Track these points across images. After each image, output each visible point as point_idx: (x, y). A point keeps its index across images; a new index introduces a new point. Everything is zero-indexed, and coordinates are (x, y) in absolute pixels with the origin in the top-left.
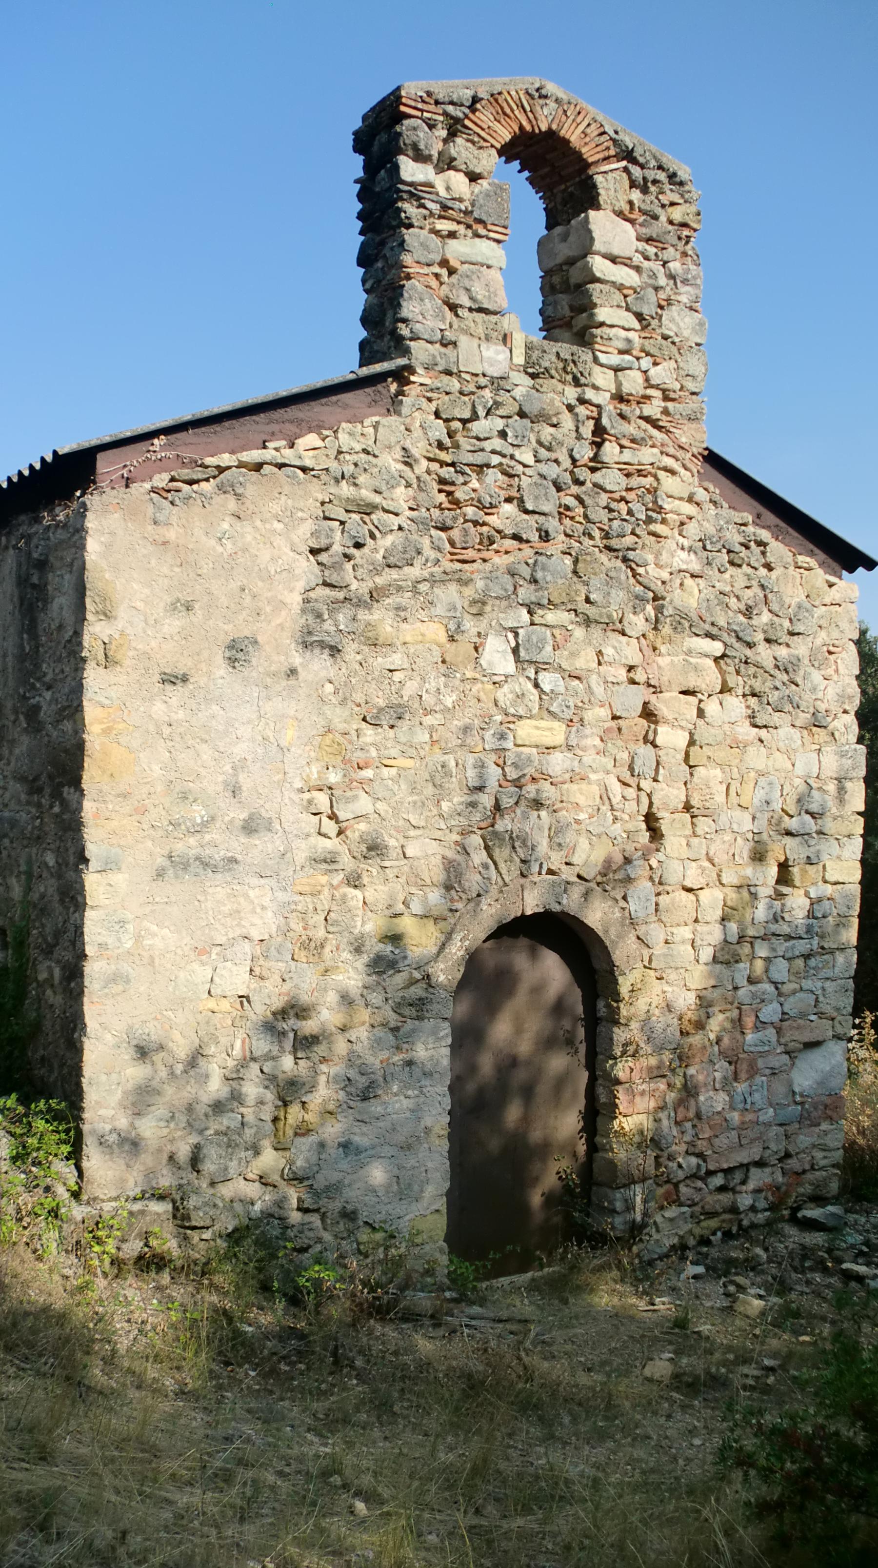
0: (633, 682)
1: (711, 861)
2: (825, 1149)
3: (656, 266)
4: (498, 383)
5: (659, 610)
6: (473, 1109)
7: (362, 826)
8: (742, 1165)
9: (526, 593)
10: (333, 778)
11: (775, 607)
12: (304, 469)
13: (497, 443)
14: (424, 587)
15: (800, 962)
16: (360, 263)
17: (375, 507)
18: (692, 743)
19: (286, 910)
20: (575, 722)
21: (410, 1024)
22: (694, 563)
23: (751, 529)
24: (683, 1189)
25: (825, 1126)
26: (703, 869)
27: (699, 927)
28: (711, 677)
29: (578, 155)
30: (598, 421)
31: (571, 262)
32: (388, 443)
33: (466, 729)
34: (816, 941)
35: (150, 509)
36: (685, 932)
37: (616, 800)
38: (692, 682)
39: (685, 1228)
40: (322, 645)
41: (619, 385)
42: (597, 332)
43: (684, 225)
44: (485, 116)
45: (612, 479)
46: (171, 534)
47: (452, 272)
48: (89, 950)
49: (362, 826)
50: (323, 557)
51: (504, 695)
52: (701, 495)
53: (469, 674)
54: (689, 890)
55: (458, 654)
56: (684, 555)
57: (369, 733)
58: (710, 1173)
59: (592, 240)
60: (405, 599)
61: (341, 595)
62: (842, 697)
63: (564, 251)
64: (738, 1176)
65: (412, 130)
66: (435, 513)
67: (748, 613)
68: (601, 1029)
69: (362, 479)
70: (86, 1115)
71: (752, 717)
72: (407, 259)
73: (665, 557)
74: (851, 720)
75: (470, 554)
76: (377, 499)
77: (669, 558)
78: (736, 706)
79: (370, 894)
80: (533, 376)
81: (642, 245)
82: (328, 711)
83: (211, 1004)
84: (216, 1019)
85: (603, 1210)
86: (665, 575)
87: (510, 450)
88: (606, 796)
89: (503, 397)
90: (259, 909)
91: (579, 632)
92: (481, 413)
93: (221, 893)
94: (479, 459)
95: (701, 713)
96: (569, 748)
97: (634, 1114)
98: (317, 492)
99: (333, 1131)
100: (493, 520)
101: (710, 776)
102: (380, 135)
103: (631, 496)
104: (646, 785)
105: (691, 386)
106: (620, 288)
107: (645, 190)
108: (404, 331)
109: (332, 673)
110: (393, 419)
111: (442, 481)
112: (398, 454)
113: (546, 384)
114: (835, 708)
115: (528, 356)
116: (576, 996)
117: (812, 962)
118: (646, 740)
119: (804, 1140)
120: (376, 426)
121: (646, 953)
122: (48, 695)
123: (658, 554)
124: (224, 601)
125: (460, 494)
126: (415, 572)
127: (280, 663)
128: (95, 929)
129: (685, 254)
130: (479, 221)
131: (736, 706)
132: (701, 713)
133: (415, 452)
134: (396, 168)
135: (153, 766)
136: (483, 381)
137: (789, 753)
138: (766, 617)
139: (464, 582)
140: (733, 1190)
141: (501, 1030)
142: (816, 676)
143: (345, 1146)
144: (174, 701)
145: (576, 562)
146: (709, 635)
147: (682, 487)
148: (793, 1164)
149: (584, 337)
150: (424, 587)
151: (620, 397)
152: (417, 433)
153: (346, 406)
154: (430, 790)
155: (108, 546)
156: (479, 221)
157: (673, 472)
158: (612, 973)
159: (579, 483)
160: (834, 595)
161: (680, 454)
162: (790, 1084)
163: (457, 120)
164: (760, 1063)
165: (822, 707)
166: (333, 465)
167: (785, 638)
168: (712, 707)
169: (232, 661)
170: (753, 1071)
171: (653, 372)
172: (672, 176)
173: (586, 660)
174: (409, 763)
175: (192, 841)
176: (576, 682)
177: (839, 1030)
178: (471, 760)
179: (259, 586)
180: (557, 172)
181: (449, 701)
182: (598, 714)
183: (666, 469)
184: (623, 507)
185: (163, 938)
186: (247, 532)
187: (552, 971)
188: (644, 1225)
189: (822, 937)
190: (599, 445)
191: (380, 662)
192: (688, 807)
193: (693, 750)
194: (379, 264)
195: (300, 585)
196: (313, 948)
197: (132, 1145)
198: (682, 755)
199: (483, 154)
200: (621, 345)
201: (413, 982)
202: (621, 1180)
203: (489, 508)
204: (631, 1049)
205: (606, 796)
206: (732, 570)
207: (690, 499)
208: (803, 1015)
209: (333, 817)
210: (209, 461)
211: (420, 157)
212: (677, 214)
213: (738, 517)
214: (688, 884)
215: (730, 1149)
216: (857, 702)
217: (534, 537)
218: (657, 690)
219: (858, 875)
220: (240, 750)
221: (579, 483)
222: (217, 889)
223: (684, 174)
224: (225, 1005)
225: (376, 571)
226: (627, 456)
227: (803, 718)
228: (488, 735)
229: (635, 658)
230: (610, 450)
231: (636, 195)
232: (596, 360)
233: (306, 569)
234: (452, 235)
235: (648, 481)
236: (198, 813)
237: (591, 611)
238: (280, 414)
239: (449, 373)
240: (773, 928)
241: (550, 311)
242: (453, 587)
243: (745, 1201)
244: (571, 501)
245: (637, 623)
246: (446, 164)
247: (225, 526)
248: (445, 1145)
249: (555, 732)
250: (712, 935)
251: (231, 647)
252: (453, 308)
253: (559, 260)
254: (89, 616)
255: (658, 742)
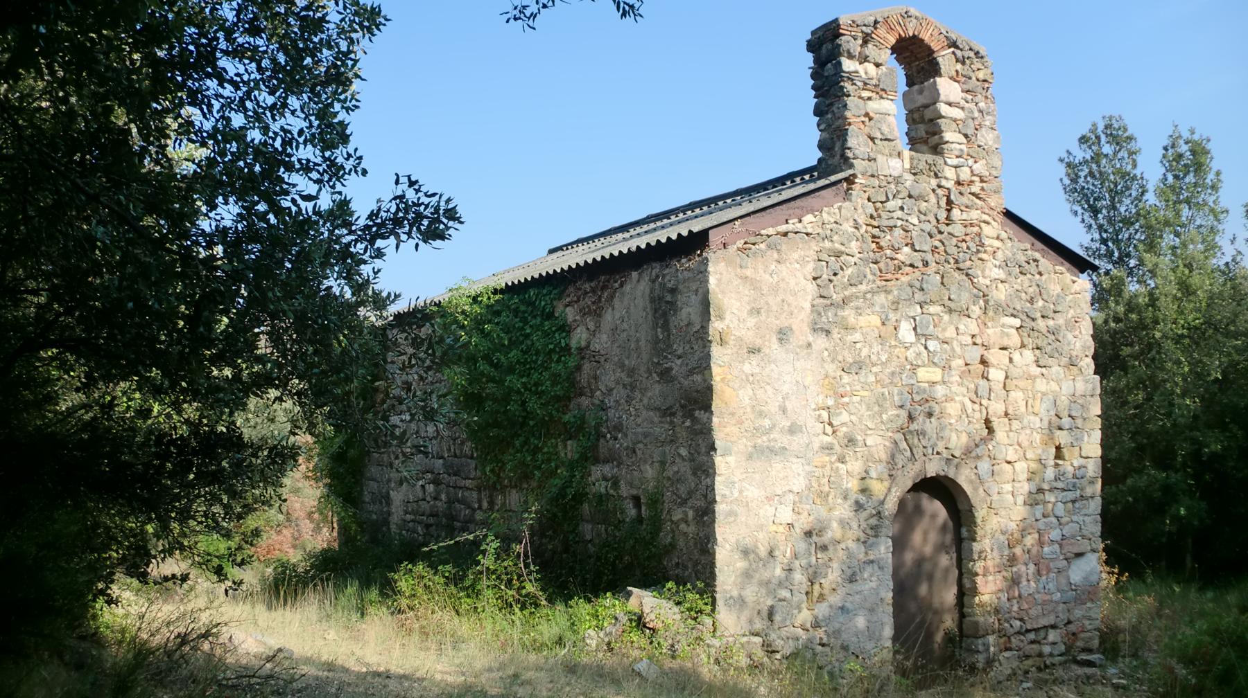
0: (975, 344)
1: (1019, 445)
2: (1090, 618)
3: (972, 106)
4: (898, 180)
5: (986, 302)
6: (904, 588)
7: (844, 429)
8: (1045, 627)
9: (919, 296)
10: (830, 402)
11: (1045, 297)
12: (807, 234)
13: (899, 214)
14: (869, 296)
15: (1070, 505)
16: (816, 114)
17: (842, 253)
18: (1007, 377)
19: (810, 474)
20: (946, 368)
21: (872, 540)
22: (1001, 274)
23: (1029, 252)
24: (1013, 639)
25: (1089, 605)
26: (1016, 451)
27: (1017, 485)
28: (1015, 340)
29: (929, 48)
30: (948, 197)
31: (926, 106)
32: (839, 217)
33: (893, 373)
34: (1078, 492)
35: (738, 260)
36: (1008, 487)
37: (969, 411)
38: (1006, 343)
39: (1015, 664)
40: (822, 329)
41: (958, 176)
42: (945, 146)
43: (985, 81)
44: (882, 31)
45: (957, 229)
46: (749, 273)
47: (870, 119)
48: (718, 498)
49: (844, 429)
50: (819, 281)
51: (911, 354)
52: (1004, 235)
53: (893, 343)
54: (1009, 463)
55: (889, 330)
56: (996, 270)
57: (845, 376)
58: (1028, 631)
59: (939, 94)
60: (860, 303)
61: (828, 302)
62: (1084, 348)
63: (921, 100)
64: (1042, 633)
65: (850, 42)
66: (871, 254)
67: (1031, 301)
68: (965, 544)
69: (835, 238)
70: (717, 589)
71: (1037, 361)
72: (848, 114)
73: (987, 272)
74: (1090, 361)
75: (889, 276)
76: (843, 248)
77: (990, 272)
78: (1029, 355)
79: (849, 466)
80: (915, 174)
81: (964, 95)
82: (826, 365)
83: (774, 528)
84: (779, 537)
85: (969, 650)
86: (988, 283)
87: (906, 217)
88: (964, 409)
89: (900, 188)
90: (794, 475)
91: (946, 317)
92: (891, 197)
93: (779, 466)
94: (891, 223)
95: (1011, 360)
96: (944, 382)
97: (989, 589)
98: (815, 246)
99: (835, 599)
100: (898, 256)
101: (1016, 395)
102: (825, 45)
103: (968, 238)
104: (984, 402)
105: (995, 173)
106: (955, 120)
107: (963, 63)
108: (849, 154)
109: (827, 345)
110: (847, 203)
111: (874, 237)
112: (851, 223)
113: (921, 178)
114: (1081, 355)
115: (911, 164)
116: (950, 524)
117: (1077, 505)
118: (983, 377)
119: (1078, 613)
120: (840, 208)
121: (988, 499)
122: (679, 362)
123: (983, 271)
124: (775, 308)
125: (882, 244)
126: (863, 287)
127: (802, 340)
128: (721, 486)
129: (986, 97)
130: (883, 90)
131: (1029, 355)
132: (1011, 360)
133: (860, 221)
134: (840, 64)
135: (745, 396)
136: (890, 179)
137: (1058, 382)
138: (1041, 303)
139: (887, 292)
140: (1039, 642)
141: (917, 537)
142: (1070, 336)
143: (842, 608)
144: (754, 363)
145: (943, 277)
146: (1013, 315)
147: (994, 230)
148: (1072, 628)
149: (937, 149)
150: (869, 296)
151: (958, 183)
152: (860, 211)
153: (824, 198)
154: (876, 408)
155: (719, 280)
156: (883, 90)
157: (988, 223)
158: (971, 511)
159: (940, 233)
160: (1076, 287)
161: (991, 212)
162: (1068, 578)
163: (867, 35)
164: (1051, 565)
165: (1074, 353)
166: (820, 231)
167: (1051, 315)
168: (1016, 356)
169: (780, 340)
170: (1049, 570)
171: (975, 167)
172: (977, 53)
173: (950, 333)
174: (866, 393)
175: (765, 438)
176: (946, 346)
177: (1094, 546)
178: (896, 391)
179: (790, 299)
180: (917, 58)
181: (884, 358)
182: (958, 363)
183: (985, 222)
184: (964, 245)
185: (753, 492)
186: (784, 270)
187: (937, 509)
188: (994, 660)
189: (1082, 490)
190: (949, 211)
191: (850, 338)
192: (1006, 414)
193: (1008, 381)
194: (829, 116)
195: (810, 298)
196: (823, 496)
197: (741, 602)
198: (1001, 385)
199: (882, 52)
200: (957, 153)
201: (872, 516)
202: (981, 633)
203: (896, 250)
204: (983, 555)
205: (964, 409)
206: (1022, 277)
207: (998, 238)
208: (1073, 537)
209: (830, 424)
210: (763, 232)
211: (851, 57)
212: (981, 75)
213: (1023, 246)
214: (1009, 459)
215: (1038, 616)
216: (1093, 350)
217: (920, 264)
218: (986, 347)
219: (1099, 453)
220: (786, 388)
221: (940, 233)
222: (777, 466)
223: (982, 53)
224: (781, 529)
225: (845, 288)
226: (965, 216)
227: (1065, 360)
228: (904, 376)
229: (975, 330)
230: (956, 213)
231: (959, 66)
232: (946, 163)
233: (811, 287)
234: (869, 99)
235: (976, 229)
236: (767, 423)
237: (952, 305)
238: (792, 204)
239: (873, 176)
240: (1055, 484)
241: (913, 134)
242: (883, 295)
243: (1047, 649)
244: (937, 243)
245: (976, 310)
246: (864, 59)
247: (773, 267)
248: (891, 609)
249: (935, 374)
250: (1025, 487)
251: (780, 333)
252: (872, 139)
253: (918, 104)
254: (712, 318)
255: (990, 377)
